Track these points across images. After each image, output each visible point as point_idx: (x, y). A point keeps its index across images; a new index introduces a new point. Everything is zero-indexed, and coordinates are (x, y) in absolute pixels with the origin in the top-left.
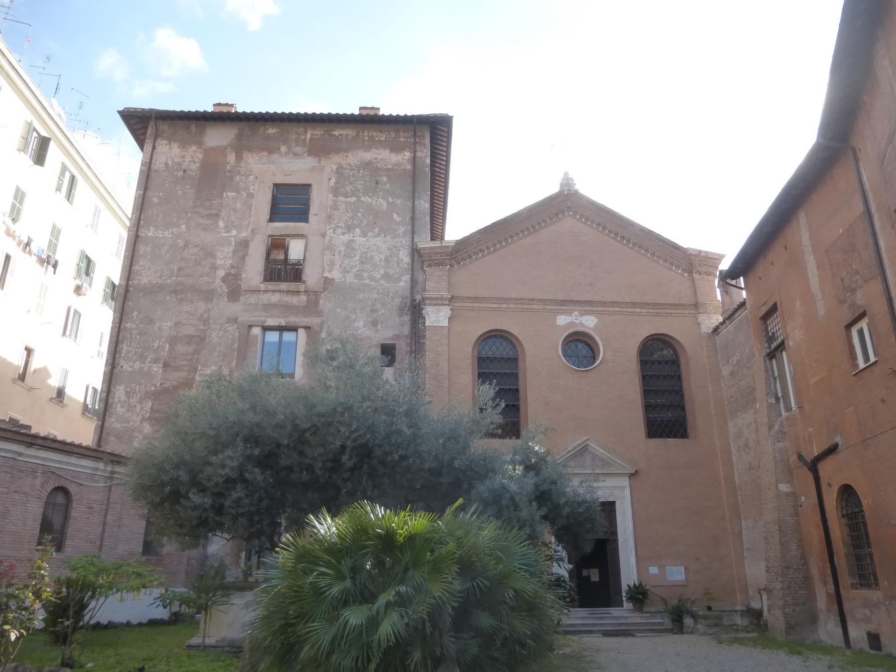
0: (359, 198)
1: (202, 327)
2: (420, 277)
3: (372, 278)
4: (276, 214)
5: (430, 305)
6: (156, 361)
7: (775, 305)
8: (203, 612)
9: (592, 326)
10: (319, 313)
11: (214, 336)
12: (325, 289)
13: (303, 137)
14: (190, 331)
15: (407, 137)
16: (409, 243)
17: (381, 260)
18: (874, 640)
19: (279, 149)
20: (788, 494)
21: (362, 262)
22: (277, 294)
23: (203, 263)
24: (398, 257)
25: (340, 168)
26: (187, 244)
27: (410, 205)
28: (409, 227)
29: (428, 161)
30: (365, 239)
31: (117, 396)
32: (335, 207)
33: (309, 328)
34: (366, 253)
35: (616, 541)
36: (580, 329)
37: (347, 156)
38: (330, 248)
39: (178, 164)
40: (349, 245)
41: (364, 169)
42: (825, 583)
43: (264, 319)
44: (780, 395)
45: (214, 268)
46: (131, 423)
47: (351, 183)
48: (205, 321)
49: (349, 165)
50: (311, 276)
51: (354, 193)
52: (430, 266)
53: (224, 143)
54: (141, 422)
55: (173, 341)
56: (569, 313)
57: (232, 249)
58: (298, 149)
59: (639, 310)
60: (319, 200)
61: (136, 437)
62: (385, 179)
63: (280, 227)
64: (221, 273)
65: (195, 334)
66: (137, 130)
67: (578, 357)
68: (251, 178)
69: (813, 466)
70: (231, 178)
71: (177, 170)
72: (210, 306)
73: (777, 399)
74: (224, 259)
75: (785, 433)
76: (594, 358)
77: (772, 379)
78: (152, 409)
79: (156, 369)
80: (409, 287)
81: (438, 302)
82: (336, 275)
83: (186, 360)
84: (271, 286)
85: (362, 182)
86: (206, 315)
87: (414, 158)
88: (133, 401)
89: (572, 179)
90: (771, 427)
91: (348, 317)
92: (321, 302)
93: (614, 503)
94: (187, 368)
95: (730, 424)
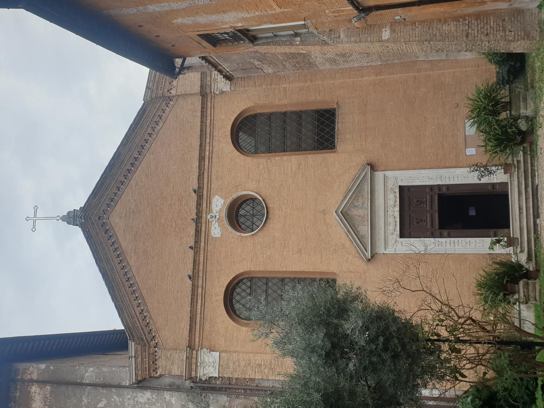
2: (167, 381)
5: (196, 372)
8: (468, 362)
16: (130, 391)
20: (393, 31)
24: (145, 403)
27: (89, 388)
28: (114, 390)
35: (439, 187)
36: (224, 214)
52: (155, 370)
56: (208, 223)
59: (207, 153)
66: (113, 336)
67: (253, 215)
73: (296, 35)
75: (330, 30)
76: (254, 199)
80: (176, 394)
81: (191, 362)
87: (37, 382)
89: (69, 213)
90: (325, 43)
93: (400, 187)
95: (322, 68)
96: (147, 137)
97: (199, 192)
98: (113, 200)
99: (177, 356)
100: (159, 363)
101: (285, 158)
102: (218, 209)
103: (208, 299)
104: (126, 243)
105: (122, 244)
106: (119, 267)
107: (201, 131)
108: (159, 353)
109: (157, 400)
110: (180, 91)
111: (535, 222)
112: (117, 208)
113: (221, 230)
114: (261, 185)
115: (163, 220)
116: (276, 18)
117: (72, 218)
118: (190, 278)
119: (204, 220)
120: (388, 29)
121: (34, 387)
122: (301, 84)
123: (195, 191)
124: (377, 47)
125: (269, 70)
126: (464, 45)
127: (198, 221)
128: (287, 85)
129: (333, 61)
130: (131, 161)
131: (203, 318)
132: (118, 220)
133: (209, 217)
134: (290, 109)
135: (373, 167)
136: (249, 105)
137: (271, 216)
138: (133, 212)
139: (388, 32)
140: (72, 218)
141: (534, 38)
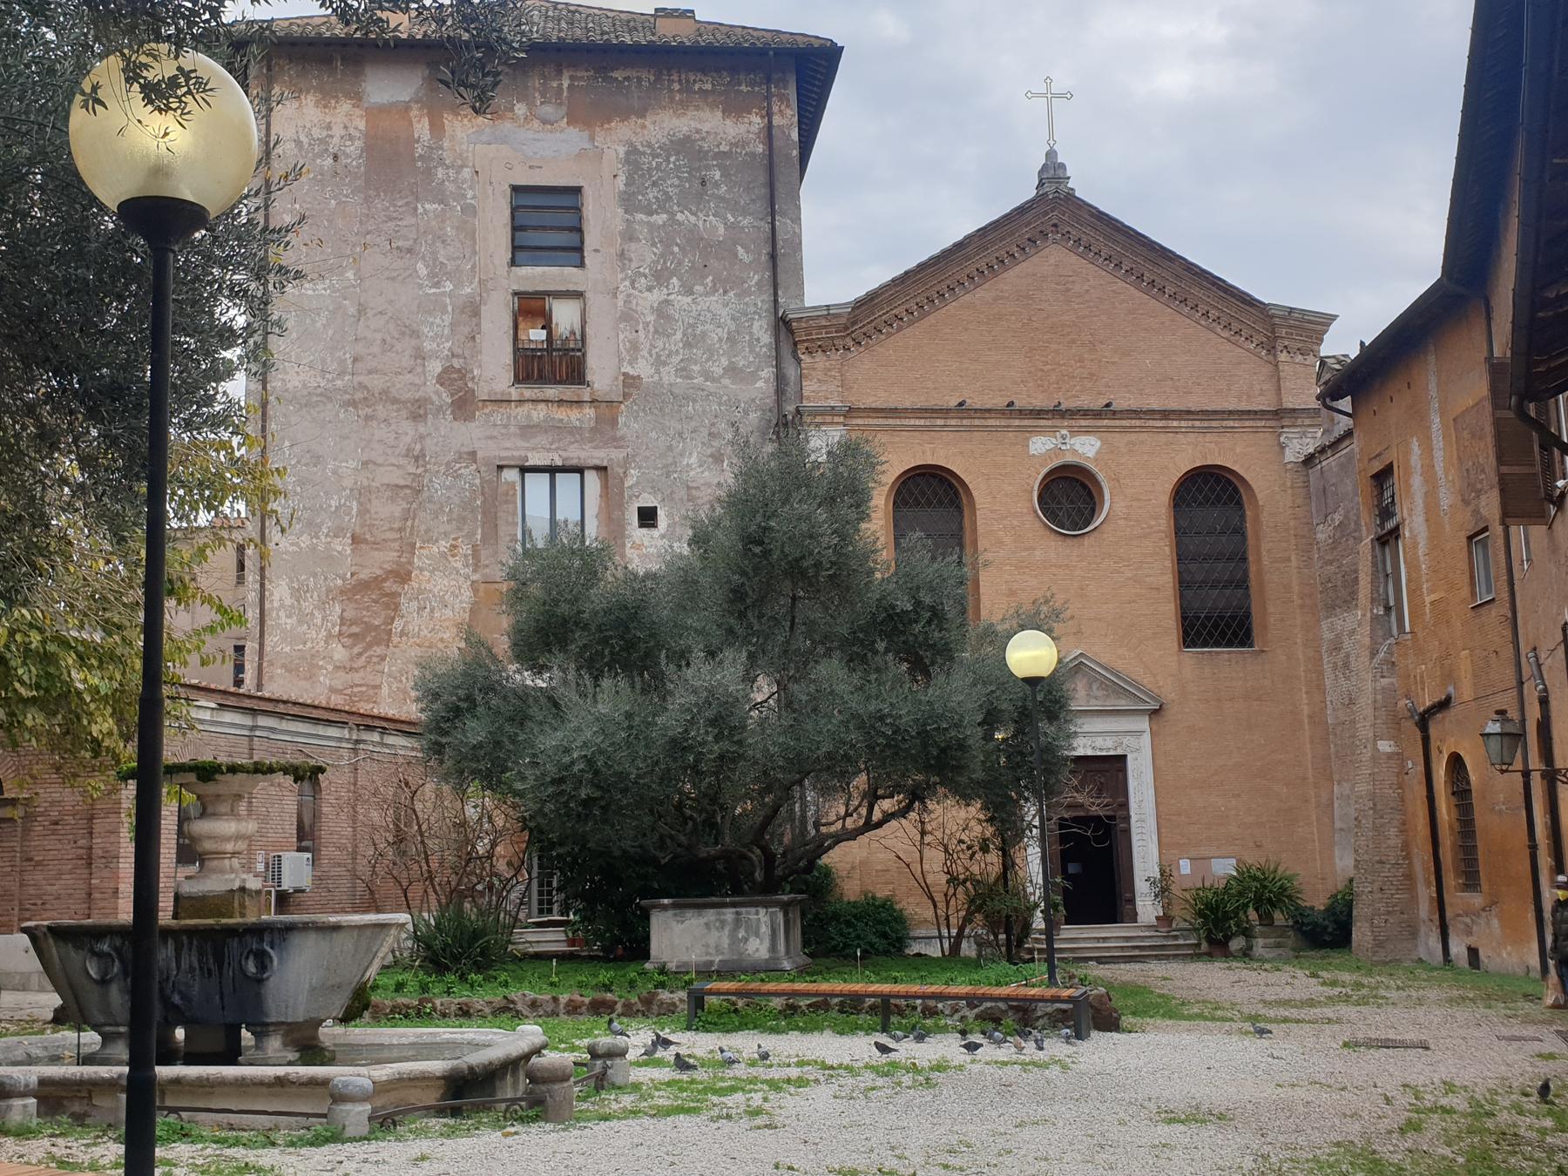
0: (672, 214)
1: (413, 470)
2: (791, 371)
3: (708, 376)
4: (520, 252)
6: (337, 532)
7: (1391, 466)
9: (1091, 455)
10: (617, 442)
11: (438, 486)
12: (626, 396)
13: (555, 84)
14: (396, 477)
15: (752, 84)
16: (768, 306)
17: (720, 340)
18: (1473, 952)
19: (512, 110)
20: (1390, 756)
21: (688, 345)
22: (542, 407)
23: (399, 347)
24: (751, 334)
25: (633, 151)
26: (362, 310)
27: (768, 228)
29: (795, 135)
30: (689, 299)
31: (276, 596)
32: (629, 236)
33: (605, 468)
34: (693, 326)
35: (1127, 818)
36: (1069, 459)
37: (644, 127)
38: (628, 317)
39: (322, 141)
40: (662, 311)
41: (678, 153)
42: (1428, 885)
43: (523, 453)
44: (1392, 603)
45: (420, 356)
46: (309, 645)
47: (654, 184)
48: (417, 459)
49: (649, 145)
50: (601, 371)
51: (663, 205)
52: (809, 351)
53: (405, 96)
54: (326, 642)
55: (363, 494)
56: (1053, 431)
57: (448, 319)
58: (548, 110)
59: (1175, 423)
60: (601, 218)
61: (321, 667)
62: (717, 175)
63: (536, 276)
64: (435, 367)
65: (402, 483)
68: (466, 173)
69: (1422, 722)
70: (429, 173)
71: (320, 155)
72: (422, 429)
73: (1388, 609)
74: (438, 337)
77: (1381, 575)
78: (342, 618)
79: (339, 548)
80: (772, 389)
82: (643, 369)
83: (391, 529)
84: (529, 392)
85: (676, 182)
86: (418, 447)
87: (770, 126)
88: (307, 606)
89: (1063, 166)
90: (1374, 653)
91: (670, 448)
92: (621, 420)
93: (1123, 758)
94: (396, 545)
95: (1325, 625)
96: (1202, 308)
97: (1107, 411)
98: (1086, 249)
99: (833, 388)
100: (819, 356)
101: (1168, 564)
102: (1077, 447)
103: (926, 436)
104: (1014, 278)
105: (1011, 272)
106: (972, 270)
107: (1215, 412)
108: (835, 356)
109: (758, 355)
110: (1286, 370)
111: (1091, 959)
112: (1074, 258)
113: (1041, 455)
114: (1121, 522)
115: (1054, 346)
116: (1414, 592)
117: (1052, 172)
118: (961, 404)
119: (1058, 422)
120: (1393, 749)
121: (758, 120)
122: (1296, 589)
123: (1108, 405)
124: (1365, 730)
125: (1323, 534)
126: (1366, 857)
127: (1058, 413)
128: (1294, 563)
129: (1336, 647)
130: (1158, 281)
131: (894, 429)
132: (1052, 261)
133: (1064, 432)
134: (1253, 569)
135: (1154, 713)
136: (1259, 496)
137: (1069, 541)
138: (1068, 290)
139: (1389, 750)
140: (1052, 172)
141: (1375, 953)
